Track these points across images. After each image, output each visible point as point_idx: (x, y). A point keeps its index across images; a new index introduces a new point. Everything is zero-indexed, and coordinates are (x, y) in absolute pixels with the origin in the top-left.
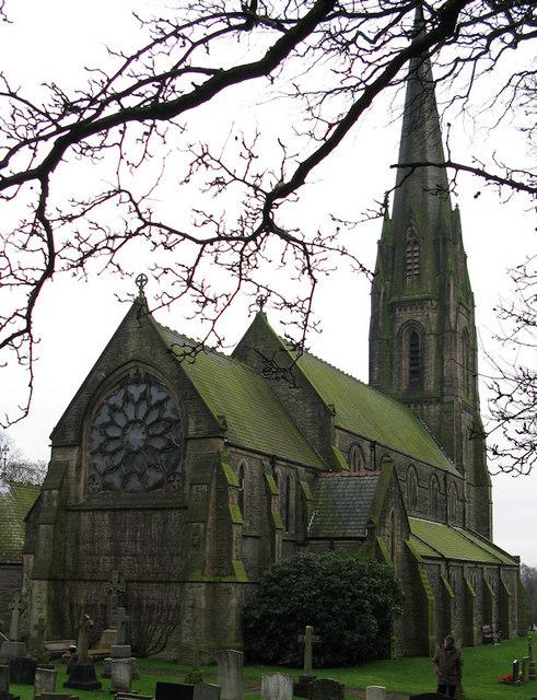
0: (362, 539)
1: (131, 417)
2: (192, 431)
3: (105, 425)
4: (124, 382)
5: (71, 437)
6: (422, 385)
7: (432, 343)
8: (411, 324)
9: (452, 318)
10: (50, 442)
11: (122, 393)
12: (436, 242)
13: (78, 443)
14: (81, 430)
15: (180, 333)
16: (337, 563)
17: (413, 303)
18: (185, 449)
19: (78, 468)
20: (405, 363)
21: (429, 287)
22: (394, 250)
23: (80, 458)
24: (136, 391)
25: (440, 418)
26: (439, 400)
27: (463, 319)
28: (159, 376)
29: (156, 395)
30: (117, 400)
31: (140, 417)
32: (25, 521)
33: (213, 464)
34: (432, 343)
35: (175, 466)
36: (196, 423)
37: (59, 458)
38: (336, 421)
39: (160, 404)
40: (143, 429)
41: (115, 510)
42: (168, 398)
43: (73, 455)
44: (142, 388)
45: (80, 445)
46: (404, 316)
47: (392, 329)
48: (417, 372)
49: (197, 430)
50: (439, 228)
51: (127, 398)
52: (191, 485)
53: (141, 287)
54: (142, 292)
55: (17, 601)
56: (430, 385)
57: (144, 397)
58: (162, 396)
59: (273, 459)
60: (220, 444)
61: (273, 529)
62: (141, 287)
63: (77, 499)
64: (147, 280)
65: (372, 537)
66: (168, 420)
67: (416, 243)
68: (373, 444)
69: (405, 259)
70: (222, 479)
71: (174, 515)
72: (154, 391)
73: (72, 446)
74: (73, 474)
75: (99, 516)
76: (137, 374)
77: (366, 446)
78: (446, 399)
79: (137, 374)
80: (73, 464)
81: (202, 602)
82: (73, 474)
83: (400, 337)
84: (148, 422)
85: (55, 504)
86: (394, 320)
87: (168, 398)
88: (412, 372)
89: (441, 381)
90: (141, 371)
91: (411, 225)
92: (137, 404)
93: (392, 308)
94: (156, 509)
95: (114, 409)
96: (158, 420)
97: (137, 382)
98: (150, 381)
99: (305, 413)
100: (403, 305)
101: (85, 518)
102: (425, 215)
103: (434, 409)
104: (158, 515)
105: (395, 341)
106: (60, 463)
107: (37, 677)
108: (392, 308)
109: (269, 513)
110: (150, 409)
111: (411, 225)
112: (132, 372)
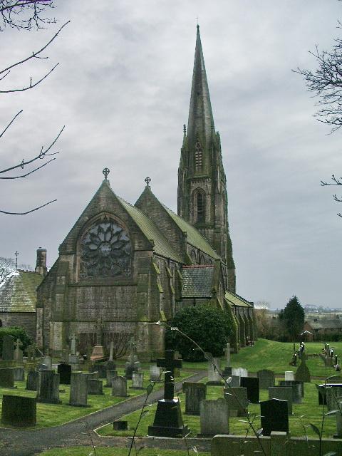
0: (210, 298)
1: (103, 240)
2: (136, 247)
3: (88, 243)
4: (99, 222)
5: (70, 249)
6: (205, 219)
7: (209, 199)
9: (219, 187)
10: (59, 252)
11: (97, 227)
12: (210, 150)
13: (74, 252)
14: (76, 248)
16: (207, 311)
17: (199, 180)
18: (133, 256)
19: (75, 265)
20: (196, 209)
21: (207, 172)
22: (189, 152)
23: (75, 259)
24: (105, 227)
25: (214, 236)
26: (213, 227)
28: (117, 219)
29: (116, 229)
30: (95, 231)
31: (108, 240)
32: (37, 291)
33: (149, 263)
34: (209, 199)
35: (127, 264)
36: (140, 243)
37: (63, 259)
38: (188, 240)
39: (118, 233)
40: (109, 246)
42: (122, 231)
43: (71, 259)
44: (108, 225)
45: (75, 254)
46: (195, 186)
47: (189, 192)
48: (202, 213)
50: (212, 143)
51: (100, 230)
52: (139, 274)
53: (106, 175)
54: (106, 177)
55: (74, 335)
56: (208, 219)
57: (110, 229)
58: (119, 229)
59: (168, 259)
60: (152, 253)
61: (171, 293)
62: (106, 175)
63: (74, 280)
64: (109, 172)
65: (214, 297)
66: (123, 241)
67: (200, 150)
68: (199, 250)
69: (195, 158)
70: (153, 271)
71: (128, 289)
72: (114, 227)
73: (70, 254)
75: (88, 289)
76: (105, 218)
77: (196, 250)
78: (217, 226)
79: (105, 218)
80: (72, 263)
81: (147, 330)
83: (193, 196)
84: (112, 242)
85: (64, 283)
86: (190, 188)
87: (122, 231)
88: (199, 213)
89: (214, 218)
90: (107, 217)
91: (198, 141)
92: (105, 233)
93: (188, 182)
95: (93, 235)
96: (118, 241)
97: (105, 222)
98: (112, 222)
99: (172, 236)
100: (195, 180)
101: (79, 290)
102: (204, 138)
103: (211, 231)
104: (120, 288)
105: (191, 198)
106: (63, 263)
107: (134, 376)
108: (188, 182)
109: (169, 287)
110: (113, 235)
111: (198, 141)
112: (102, 217)
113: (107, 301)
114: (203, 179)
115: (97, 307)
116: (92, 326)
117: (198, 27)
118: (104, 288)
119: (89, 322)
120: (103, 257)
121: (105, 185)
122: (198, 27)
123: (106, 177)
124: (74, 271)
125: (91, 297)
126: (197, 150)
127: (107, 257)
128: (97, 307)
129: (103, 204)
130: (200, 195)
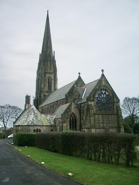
1: (103, 97)
7: (53, 81)
8: (49, 77)
15: (131, 97)
17: (50, 73)
19: (94, 106)
21: (52, 71)
24: (103, 92)
27: (40, 71)
30: (103, 92)
31: (103, 97)
34: (53, 81)
36: (116, 99)
41: (102, 115)
44: (104, 91)
46: (48, 75)
47: (45, 77)
49: (116, 101)
51: (102, 93)
53: (103, 72)
54: (103, 73)
57: (105, 93)
62: (103, 72)
68: (91, 159)
71: (113, 116)
74: (93, 107)
75: (99, 115)
80: (93, 105)
82: (93, 107)
94: (110, 115)
97: (104, 90)
98: (106, 90)
104: (110, 116)
113: (106, 120)
114: (51, 73)
115: (103, 123)
116: (102, 130)
117: (48, 11)
118: (106, 116)
119: (100, 128)
120: (103, 104)
121: (103, 75)
122: (48, 11)
123: (103, 73)
124: (94, 108)
125: (101, 119)
126: (49, 61)
127: (105, 104)
128: (103, 123)
129: (103, 83)
130: (49, 79)
